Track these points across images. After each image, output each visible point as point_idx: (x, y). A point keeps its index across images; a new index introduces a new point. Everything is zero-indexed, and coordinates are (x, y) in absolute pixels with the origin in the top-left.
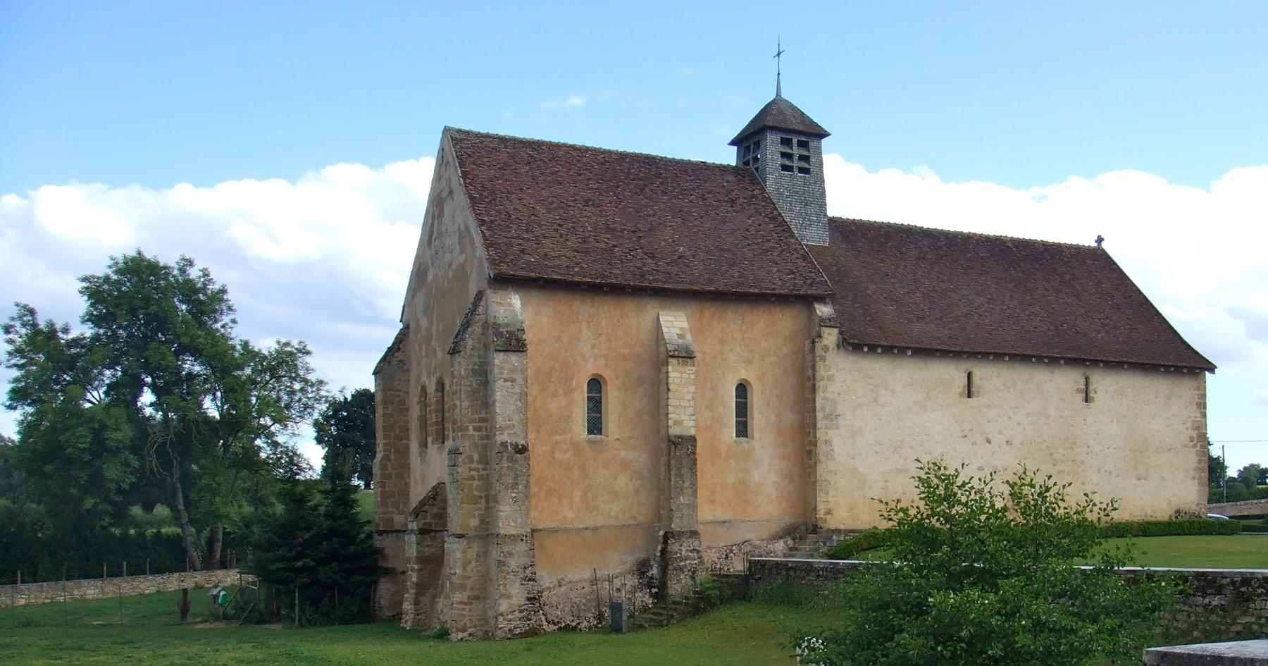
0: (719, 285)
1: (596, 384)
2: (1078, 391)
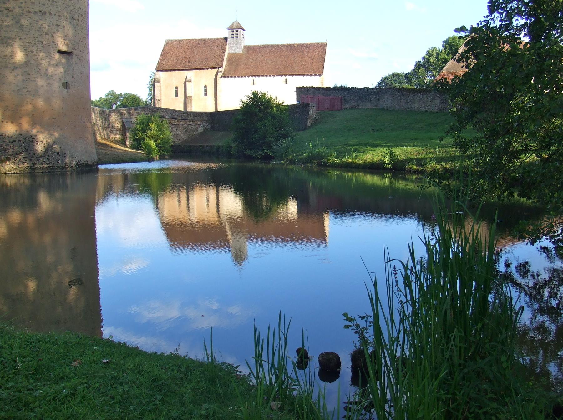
0: (198, 67)
1: (177, 88)
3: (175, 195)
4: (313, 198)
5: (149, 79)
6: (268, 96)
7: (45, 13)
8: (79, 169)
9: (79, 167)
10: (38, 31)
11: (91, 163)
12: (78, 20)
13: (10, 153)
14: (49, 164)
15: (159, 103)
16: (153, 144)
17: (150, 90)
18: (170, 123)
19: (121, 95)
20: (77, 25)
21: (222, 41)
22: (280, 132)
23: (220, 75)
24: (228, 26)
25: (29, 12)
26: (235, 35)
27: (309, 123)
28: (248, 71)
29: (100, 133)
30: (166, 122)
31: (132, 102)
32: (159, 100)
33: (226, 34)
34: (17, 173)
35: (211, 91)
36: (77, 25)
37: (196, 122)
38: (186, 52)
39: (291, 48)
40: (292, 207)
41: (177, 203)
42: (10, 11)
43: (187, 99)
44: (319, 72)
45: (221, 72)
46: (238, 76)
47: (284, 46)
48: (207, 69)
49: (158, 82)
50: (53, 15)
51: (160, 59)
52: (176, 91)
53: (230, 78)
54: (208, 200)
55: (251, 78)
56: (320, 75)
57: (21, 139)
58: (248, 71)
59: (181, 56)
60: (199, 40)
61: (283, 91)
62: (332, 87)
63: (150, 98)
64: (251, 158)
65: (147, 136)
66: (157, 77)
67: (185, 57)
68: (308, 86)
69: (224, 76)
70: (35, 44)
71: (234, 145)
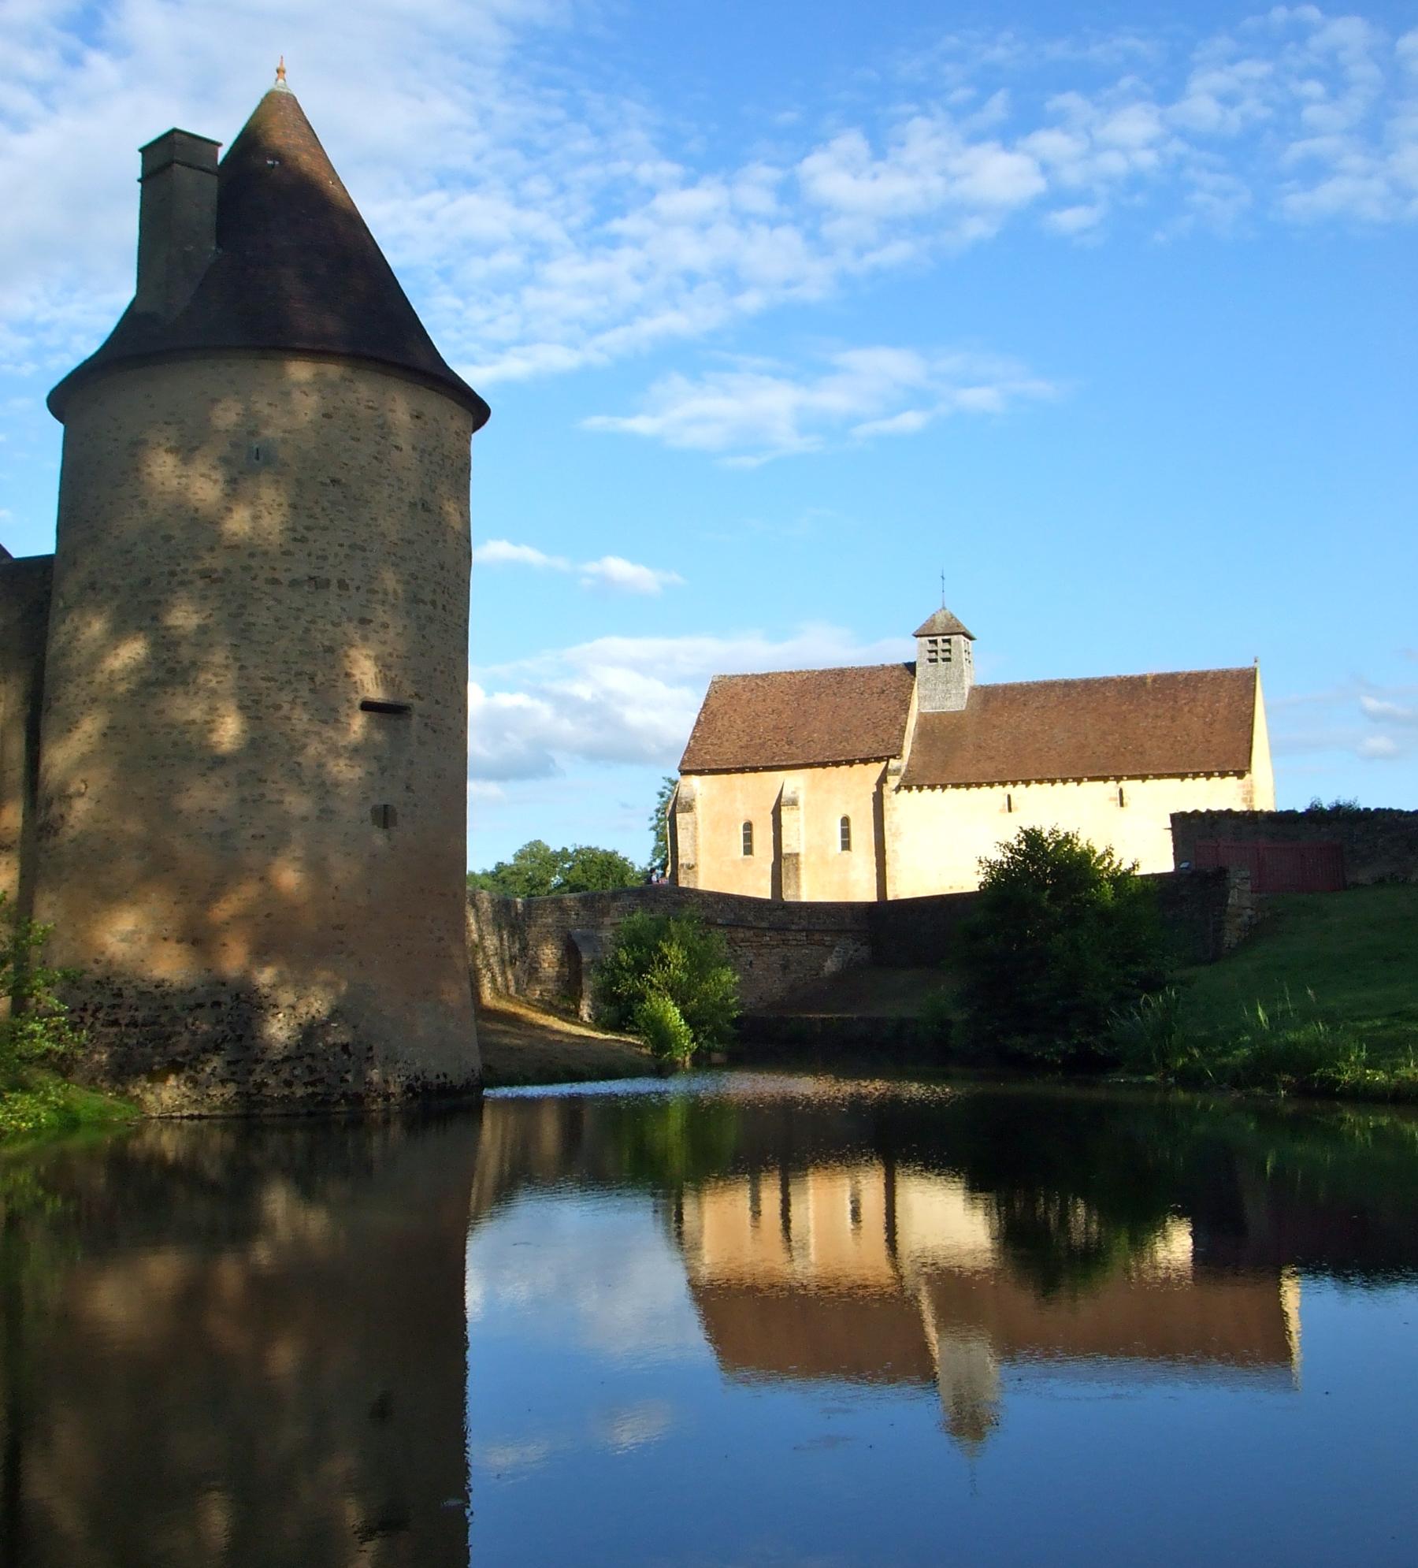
0: (820, 759)
1: (748, 826)
2: (1111, 799)
3: (740, 1198)
4: (1256, 1211)
5: (655, 802)
6: (1082, 844)
7: (327, 584)
8: (415, 1105)
9: (416, 1095)
10: (301, 640)
11: (459, 1082)
12: (434, 603)
13: (182, 1047)
14: (312, 1084)
15: (691, 877)
16: (674, 1015)
17: (660, 836)
18: (731, 942)
19: (564, 855)
20: (431, 619)
21: (896, 673)
22: (1133, 968)
23: (893, 781)
24: (915, 629)
25: (275, 582)
26: (941, 655)
27: (1231, 937)
28: (989, 767)
29: (493, 980)
30: (718, 935)
31: (597, 875)
32: (691, 867)
33: (911, 650)
34: (200, 1117)
35: (862, 834)
36: (431, 619)
37: (817, 937)
38: (780, 714)
39: (1132, 687)
40: (1177, 1245)
41: (749, 1214)
42: (214, 581)
43: (781, 864)
44: (1235, 763)
45: (896, 772)
46: (956, 786)
47: (1106, 682)
48: (851, 763)
49: (689, 808)
50: (352, 590)
51: (693, 737)
52: (748, 838)
53: (926, 792)
54: (856, 1214)
55: (998, 789)
56: (1240, 774)
57: (225, 998)
58: (989, 767)
59: (758, 727)
60: (822, 673)
61: (1130, 827)
62: (1301, 810)
63: (658, 862)
64: (1023, 1065)
65: (652, 986)
66: (684, 792)
67: (776, 727)
68: (1215, 808)
69: (907, 785)
70: (289, 682)
71: (958, 1016)
